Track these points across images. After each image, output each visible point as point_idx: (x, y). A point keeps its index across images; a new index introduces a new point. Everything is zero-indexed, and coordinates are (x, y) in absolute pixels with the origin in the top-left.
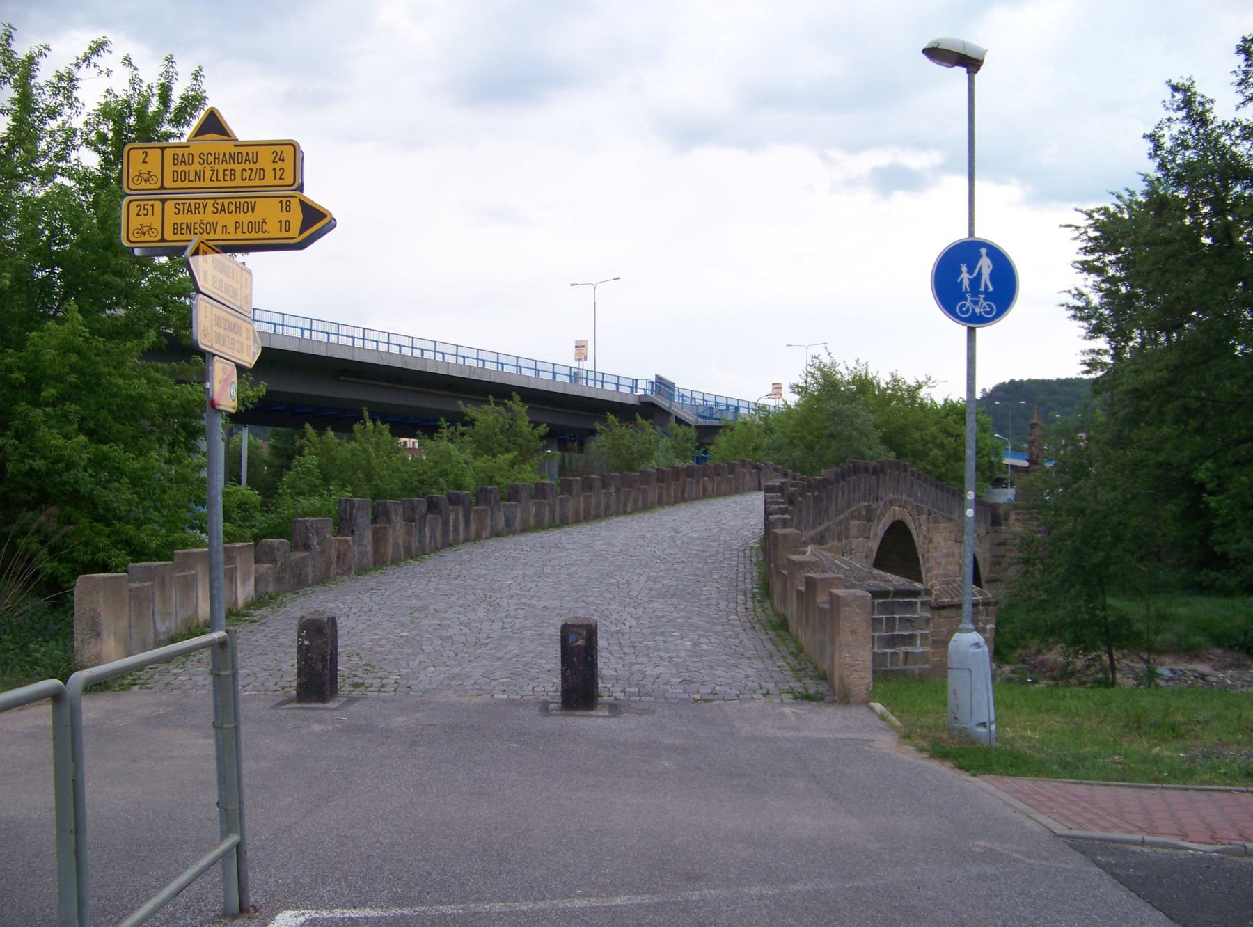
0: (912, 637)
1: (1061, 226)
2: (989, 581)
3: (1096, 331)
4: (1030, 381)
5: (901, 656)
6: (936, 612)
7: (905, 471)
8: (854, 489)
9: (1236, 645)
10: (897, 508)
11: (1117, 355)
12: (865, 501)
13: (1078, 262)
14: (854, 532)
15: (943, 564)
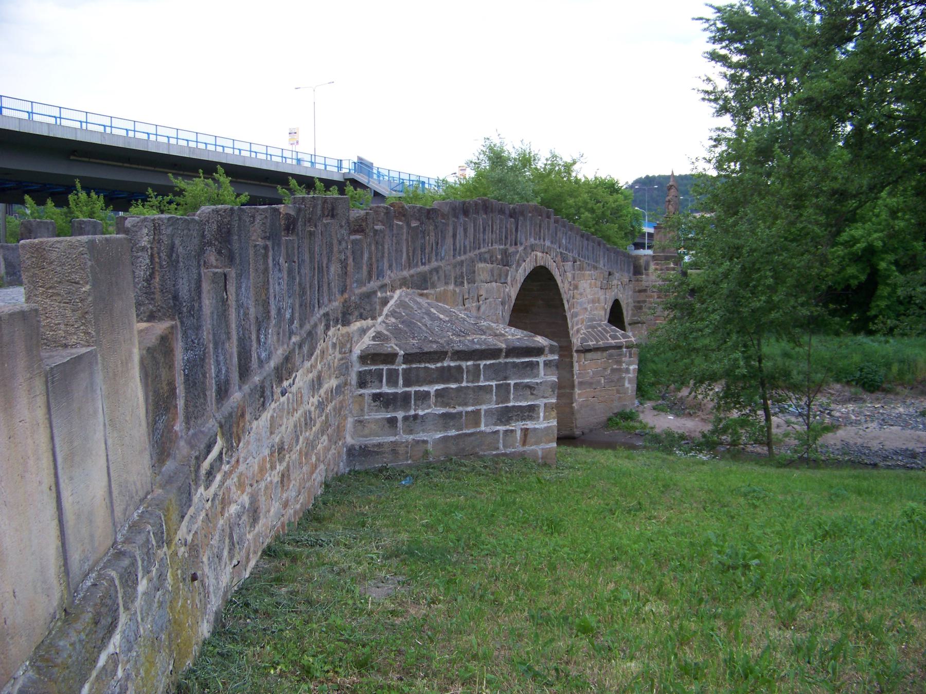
0: (532, 408)
1: (693, 19)
2: (632, 324)
3: (724, 109)
4: (660, 177)
5: (519, 433)
6: (582, 355)
7: (549, 217)
8: (484, 230)
9: (852, 380)
10: (539, 254)
11: (740, 133)
12: (501, 244)
13: (707, 53)
14: (484, 276)
15: (589, 309)
